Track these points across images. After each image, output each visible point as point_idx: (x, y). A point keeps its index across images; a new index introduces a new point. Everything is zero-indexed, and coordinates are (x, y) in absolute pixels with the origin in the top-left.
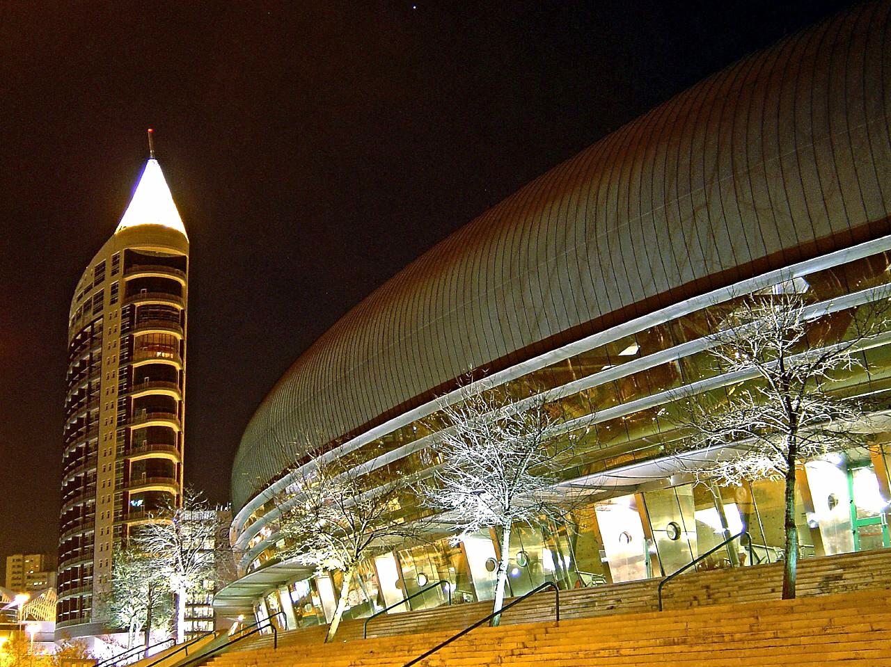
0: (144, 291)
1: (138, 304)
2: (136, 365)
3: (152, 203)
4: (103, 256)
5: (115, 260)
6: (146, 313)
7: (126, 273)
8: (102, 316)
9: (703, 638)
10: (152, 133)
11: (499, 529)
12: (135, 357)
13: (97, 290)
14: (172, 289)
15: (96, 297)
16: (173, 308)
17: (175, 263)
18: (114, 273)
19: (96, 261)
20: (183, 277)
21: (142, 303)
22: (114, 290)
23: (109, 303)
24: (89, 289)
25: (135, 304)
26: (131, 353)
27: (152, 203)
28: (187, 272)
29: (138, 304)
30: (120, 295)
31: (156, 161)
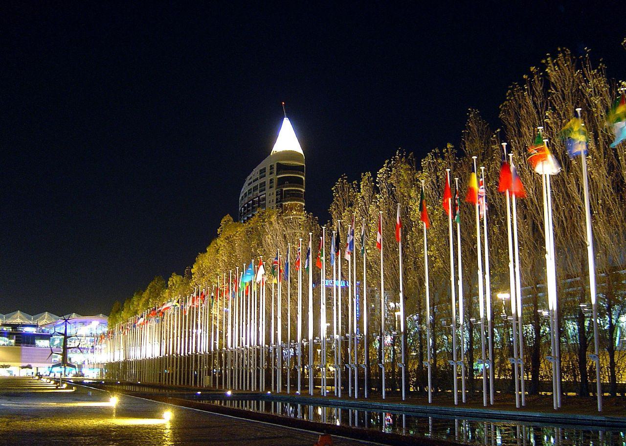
1: (284, 189)
3: (287, 140)
4: (265, 164)
5: (272, 167)
8: (265, 194)
10: (284, 105)
13: (262, 180)
14: (298, 181)
15: (261, 184)
17: (298, 169)
18: (271, 187)
19: (260, 167)
20: (303, 175)
21: (287, 189)
23: (269, 173)
24: (257, 179)
27: (287, 140)
28: (304, 184)
29: (284, 189)
30: (275, 185)
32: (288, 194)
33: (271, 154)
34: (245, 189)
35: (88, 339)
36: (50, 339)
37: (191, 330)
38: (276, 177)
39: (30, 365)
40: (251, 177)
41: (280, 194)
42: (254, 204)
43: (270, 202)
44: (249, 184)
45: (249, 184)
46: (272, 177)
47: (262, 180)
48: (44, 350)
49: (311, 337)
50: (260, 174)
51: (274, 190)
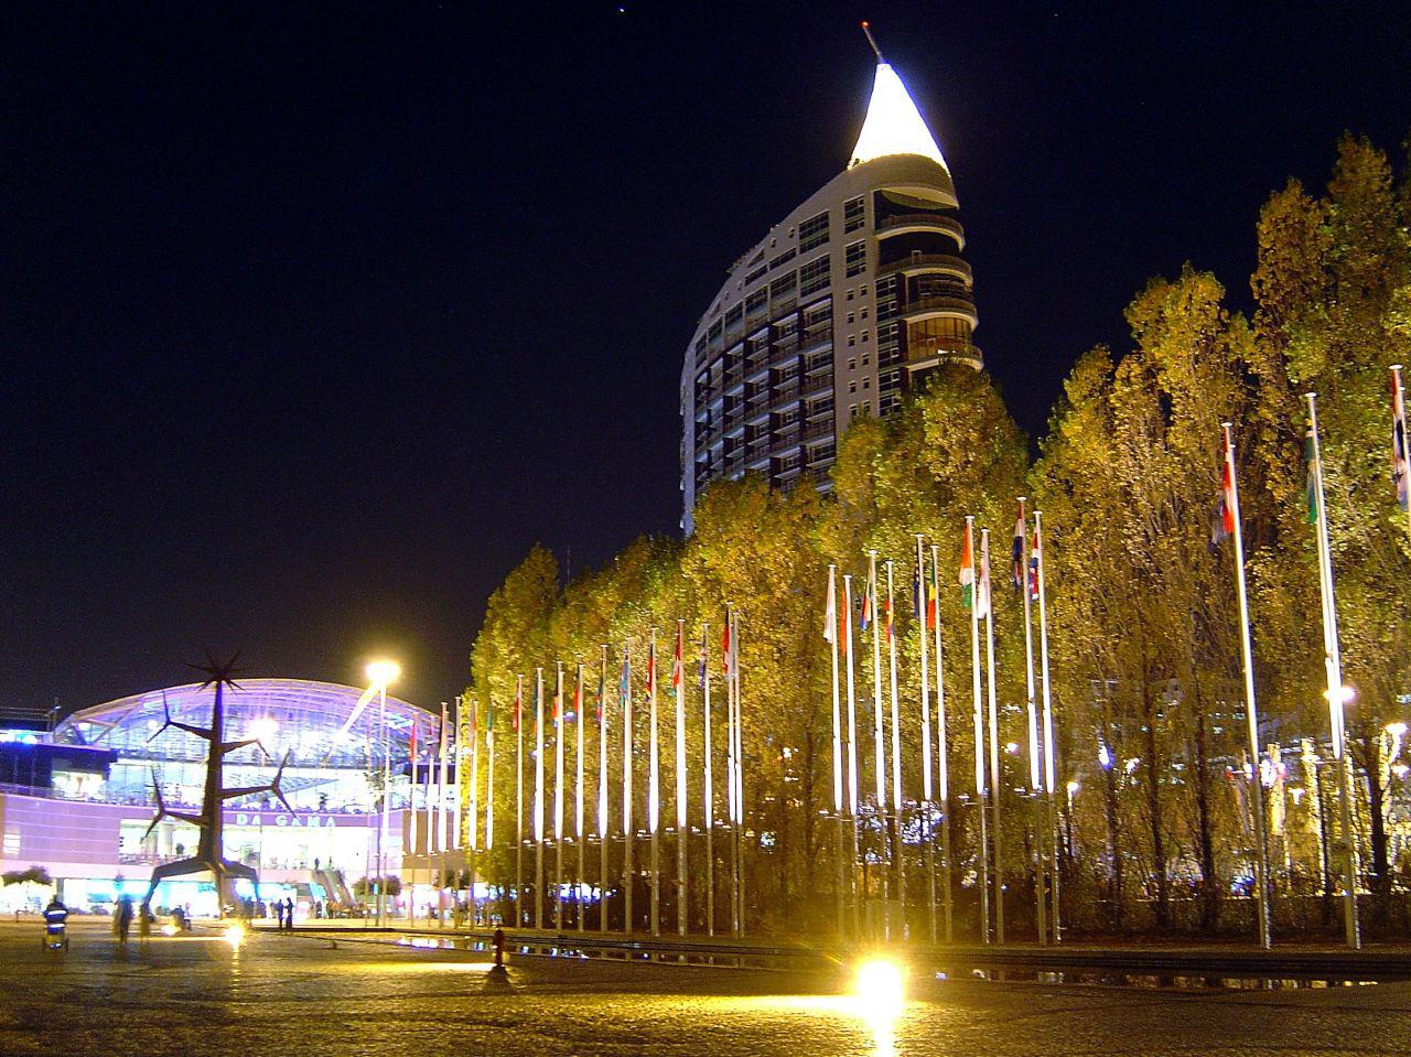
0: (917, 254)
1: (910, 273)
2: (912, 368)
3: (893, 124)
4: (827, 201)
5: (853, 209)
6: (928, 286)
7: (879, 227)
8: (830, 296)
9: (126, 1007)
10: (869, 28)
11: (379, 764)
12: (911, 355)
13: (815, 255)
16: (952, 276)
22: (854, 254)
25: (905, 273)
26: (903, 348)
27: (893, 124)
29: (910, 273)
31: (888, 66)
32: (927, 288)
33: (850, 168)
34: (733, 293)
35: (312, 751)
36: (106, 773)
37: (539, 754)
38: (870, 238)
39: (43, 870)
40: (762, 254)
41: (892, 290)
42: (752, 353)
43: (851, 320)
44: (749, 280)
45: (749, 280)
46: (855, 239)
47: (815, 255)
48: (87, 810)
49: (558, 834)
50: (802, 237)
51: (868, 280)
